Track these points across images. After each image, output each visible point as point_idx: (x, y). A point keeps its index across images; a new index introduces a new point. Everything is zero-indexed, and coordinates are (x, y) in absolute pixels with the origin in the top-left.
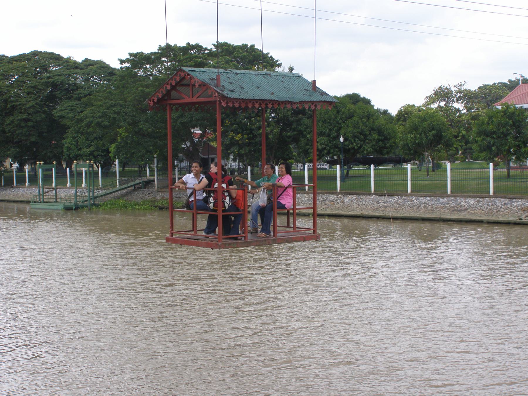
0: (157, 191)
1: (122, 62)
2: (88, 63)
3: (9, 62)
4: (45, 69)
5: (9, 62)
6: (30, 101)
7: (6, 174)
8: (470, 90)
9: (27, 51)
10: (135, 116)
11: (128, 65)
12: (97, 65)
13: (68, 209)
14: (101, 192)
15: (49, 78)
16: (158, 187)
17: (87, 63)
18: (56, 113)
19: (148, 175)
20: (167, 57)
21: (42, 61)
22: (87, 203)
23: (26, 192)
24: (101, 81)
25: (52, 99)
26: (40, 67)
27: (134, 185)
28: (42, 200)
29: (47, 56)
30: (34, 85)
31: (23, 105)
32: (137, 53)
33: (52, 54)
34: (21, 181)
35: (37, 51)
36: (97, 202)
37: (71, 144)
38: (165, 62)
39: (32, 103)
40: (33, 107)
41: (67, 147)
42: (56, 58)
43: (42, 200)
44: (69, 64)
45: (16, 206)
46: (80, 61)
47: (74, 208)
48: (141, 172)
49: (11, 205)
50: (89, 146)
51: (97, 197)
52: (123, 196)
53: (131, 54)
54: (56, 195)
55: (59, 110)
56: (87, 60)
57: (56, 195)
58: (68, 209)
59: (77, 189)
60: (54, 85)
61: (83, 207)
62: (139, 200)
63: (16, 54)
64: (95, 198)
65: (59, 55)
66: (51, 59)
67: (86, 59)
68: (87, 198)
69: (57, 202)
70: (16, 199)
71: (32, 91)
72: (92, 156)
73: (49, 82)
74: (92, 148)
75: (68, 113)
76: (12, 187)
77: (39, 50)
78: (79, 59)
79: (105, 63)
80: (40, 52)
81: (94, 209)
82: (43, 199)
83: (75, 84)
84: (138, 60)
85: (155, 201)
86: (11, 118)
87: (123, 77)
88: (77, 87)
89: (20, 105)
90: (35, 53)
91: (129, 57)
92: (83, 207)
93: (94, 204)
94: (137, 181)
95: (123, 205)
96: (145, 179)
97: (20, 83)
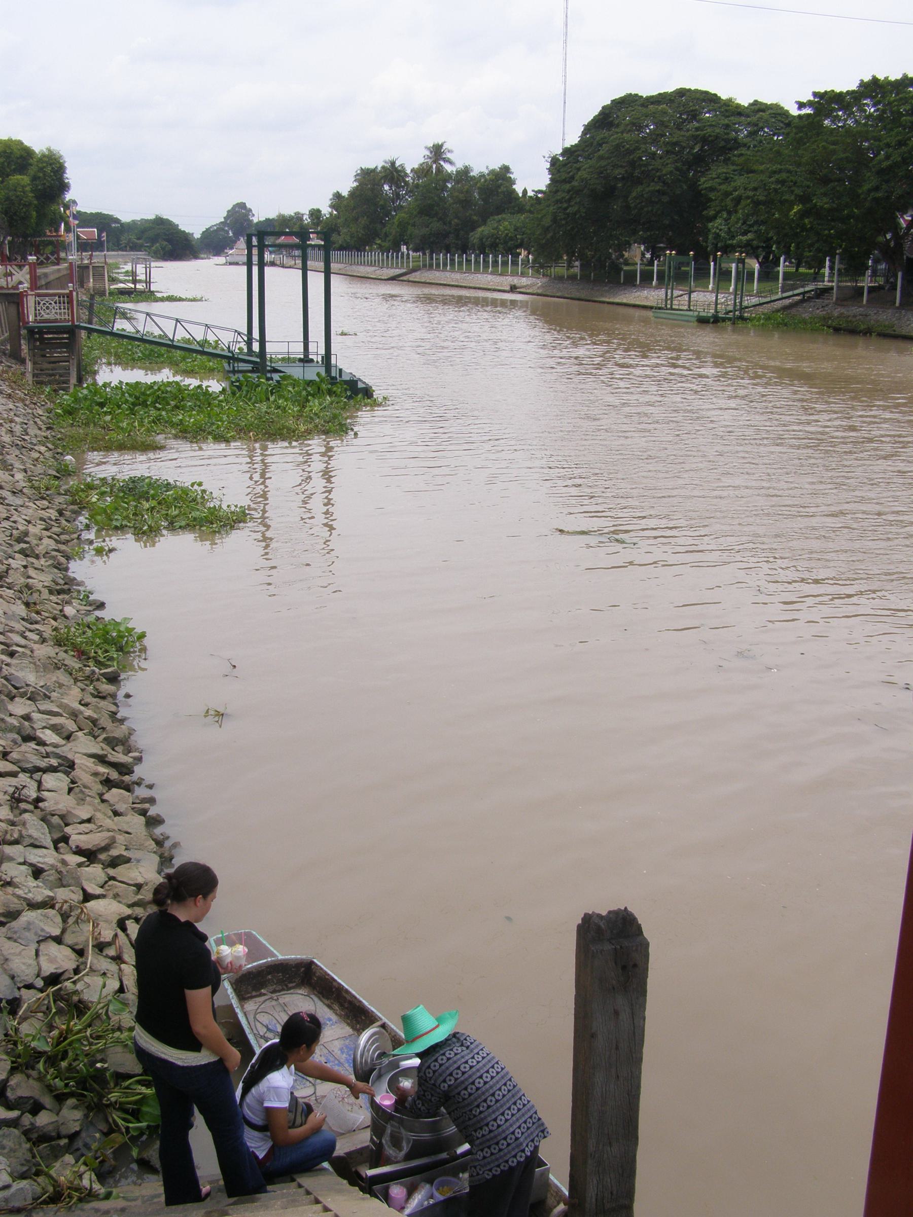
0: (836, 303)
1: (801, 105)
2: (758, 107)
3: (643, 105)
4: (694, 115)
5: (643, 105)
6: (667, 164)
7: (625, 268)
8: (833, 91)
9: (670, 88)
10: (808, 187)
11: (808, 111)
12: (770, 111)
13: (703, 321)
14: (755, 301)
15: (697, 129)
16: (837, 299)
17: (756, 108)
18: (704, 182)
19: (826, 279)
20: (872, 98)
21: (691, 104)
22: (731, 315)
23: (653, 296)
24: (774, 135)
25: (699, 161)
26: (688, 113)
27: (804, 293)
28: (669, 306)
29: (698, 96)
30: (674, 140)
31: (658, 170)
32: (826, 92)
33: (706, 93)
34: (647, 278)
35: (685, 89)
36: (746, 315)
37: (721, 230)
38: (868, 105)
39: (670, 168)
40: (671, 172)
41: (715, 233)
42: (711, 99)
43: (669, 306)
44: (729, 109)
45: (638, 313)
46: (746, 105)
47: (712, 320)
48: (817, 277)
49: (631, 311)
50: (745, 233)
51: (747, 307)
52: (785, 308)
53: (815, 94)
54: (689, 301)
55: (709, 179)
56: (756, 103)
57: (689, 301)
58: (703, 321)
59: (718, 293)
60: (704, 140)
61: (724, 320)
62: (806, 316)
63: (654, 93)
64: (742, 309)
65: (715, 95)
66: (704, 101)
67: (756, 101)
68: (731, 308)
69: (690, 310)
70: (637, 303)
71: (672, 149)
72: (751, 250)
73: (698, 136)
74: (750, 236)
75: (720, 184)
76: (635, 286)
77: (687, 88)
78: (744, 100)
79: (782, 108)
80: (689, 90)
81: (740, 324)
82: (671, 305)
83: (736, 140)
84: (826, 102)
85: (829, 318)
86: (639, 189)
87: (800, 129)
88: (737, 144)
89: (653, 169)
90: (681, 93)
91: (812, 98)
92: (724, 320)
93: (742, 318)
94: (807, 289)
95: (784, 321)
96: (820, 285)
97: (655, 138)
